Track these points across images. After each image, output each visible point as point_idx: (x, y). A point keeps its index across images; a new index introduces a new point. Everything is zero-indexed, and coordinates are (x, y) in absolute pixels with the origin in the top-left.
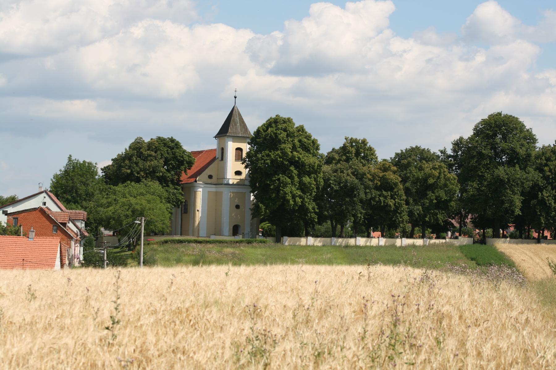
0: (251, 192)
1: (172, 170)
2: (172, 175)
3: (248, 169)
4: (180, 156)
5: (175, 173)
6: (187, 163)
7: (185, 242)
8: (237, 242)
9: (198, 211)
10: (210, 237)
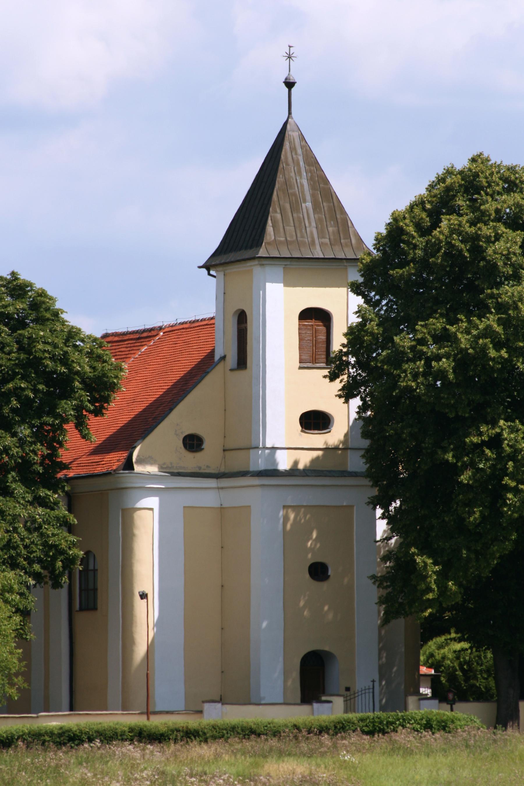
0: (374, 503)
1: (23, 421)
2: (22, 442)
3: (356, 402)
4: (53, 358)
5: (34, 435)
6: (88, 385)
7: (91, 740)
8: (322, 730)
9: (144, 596)
10: (201, 712)
